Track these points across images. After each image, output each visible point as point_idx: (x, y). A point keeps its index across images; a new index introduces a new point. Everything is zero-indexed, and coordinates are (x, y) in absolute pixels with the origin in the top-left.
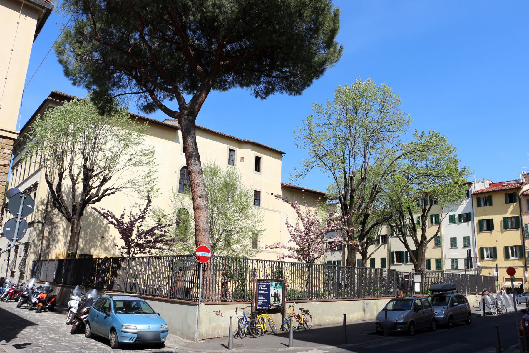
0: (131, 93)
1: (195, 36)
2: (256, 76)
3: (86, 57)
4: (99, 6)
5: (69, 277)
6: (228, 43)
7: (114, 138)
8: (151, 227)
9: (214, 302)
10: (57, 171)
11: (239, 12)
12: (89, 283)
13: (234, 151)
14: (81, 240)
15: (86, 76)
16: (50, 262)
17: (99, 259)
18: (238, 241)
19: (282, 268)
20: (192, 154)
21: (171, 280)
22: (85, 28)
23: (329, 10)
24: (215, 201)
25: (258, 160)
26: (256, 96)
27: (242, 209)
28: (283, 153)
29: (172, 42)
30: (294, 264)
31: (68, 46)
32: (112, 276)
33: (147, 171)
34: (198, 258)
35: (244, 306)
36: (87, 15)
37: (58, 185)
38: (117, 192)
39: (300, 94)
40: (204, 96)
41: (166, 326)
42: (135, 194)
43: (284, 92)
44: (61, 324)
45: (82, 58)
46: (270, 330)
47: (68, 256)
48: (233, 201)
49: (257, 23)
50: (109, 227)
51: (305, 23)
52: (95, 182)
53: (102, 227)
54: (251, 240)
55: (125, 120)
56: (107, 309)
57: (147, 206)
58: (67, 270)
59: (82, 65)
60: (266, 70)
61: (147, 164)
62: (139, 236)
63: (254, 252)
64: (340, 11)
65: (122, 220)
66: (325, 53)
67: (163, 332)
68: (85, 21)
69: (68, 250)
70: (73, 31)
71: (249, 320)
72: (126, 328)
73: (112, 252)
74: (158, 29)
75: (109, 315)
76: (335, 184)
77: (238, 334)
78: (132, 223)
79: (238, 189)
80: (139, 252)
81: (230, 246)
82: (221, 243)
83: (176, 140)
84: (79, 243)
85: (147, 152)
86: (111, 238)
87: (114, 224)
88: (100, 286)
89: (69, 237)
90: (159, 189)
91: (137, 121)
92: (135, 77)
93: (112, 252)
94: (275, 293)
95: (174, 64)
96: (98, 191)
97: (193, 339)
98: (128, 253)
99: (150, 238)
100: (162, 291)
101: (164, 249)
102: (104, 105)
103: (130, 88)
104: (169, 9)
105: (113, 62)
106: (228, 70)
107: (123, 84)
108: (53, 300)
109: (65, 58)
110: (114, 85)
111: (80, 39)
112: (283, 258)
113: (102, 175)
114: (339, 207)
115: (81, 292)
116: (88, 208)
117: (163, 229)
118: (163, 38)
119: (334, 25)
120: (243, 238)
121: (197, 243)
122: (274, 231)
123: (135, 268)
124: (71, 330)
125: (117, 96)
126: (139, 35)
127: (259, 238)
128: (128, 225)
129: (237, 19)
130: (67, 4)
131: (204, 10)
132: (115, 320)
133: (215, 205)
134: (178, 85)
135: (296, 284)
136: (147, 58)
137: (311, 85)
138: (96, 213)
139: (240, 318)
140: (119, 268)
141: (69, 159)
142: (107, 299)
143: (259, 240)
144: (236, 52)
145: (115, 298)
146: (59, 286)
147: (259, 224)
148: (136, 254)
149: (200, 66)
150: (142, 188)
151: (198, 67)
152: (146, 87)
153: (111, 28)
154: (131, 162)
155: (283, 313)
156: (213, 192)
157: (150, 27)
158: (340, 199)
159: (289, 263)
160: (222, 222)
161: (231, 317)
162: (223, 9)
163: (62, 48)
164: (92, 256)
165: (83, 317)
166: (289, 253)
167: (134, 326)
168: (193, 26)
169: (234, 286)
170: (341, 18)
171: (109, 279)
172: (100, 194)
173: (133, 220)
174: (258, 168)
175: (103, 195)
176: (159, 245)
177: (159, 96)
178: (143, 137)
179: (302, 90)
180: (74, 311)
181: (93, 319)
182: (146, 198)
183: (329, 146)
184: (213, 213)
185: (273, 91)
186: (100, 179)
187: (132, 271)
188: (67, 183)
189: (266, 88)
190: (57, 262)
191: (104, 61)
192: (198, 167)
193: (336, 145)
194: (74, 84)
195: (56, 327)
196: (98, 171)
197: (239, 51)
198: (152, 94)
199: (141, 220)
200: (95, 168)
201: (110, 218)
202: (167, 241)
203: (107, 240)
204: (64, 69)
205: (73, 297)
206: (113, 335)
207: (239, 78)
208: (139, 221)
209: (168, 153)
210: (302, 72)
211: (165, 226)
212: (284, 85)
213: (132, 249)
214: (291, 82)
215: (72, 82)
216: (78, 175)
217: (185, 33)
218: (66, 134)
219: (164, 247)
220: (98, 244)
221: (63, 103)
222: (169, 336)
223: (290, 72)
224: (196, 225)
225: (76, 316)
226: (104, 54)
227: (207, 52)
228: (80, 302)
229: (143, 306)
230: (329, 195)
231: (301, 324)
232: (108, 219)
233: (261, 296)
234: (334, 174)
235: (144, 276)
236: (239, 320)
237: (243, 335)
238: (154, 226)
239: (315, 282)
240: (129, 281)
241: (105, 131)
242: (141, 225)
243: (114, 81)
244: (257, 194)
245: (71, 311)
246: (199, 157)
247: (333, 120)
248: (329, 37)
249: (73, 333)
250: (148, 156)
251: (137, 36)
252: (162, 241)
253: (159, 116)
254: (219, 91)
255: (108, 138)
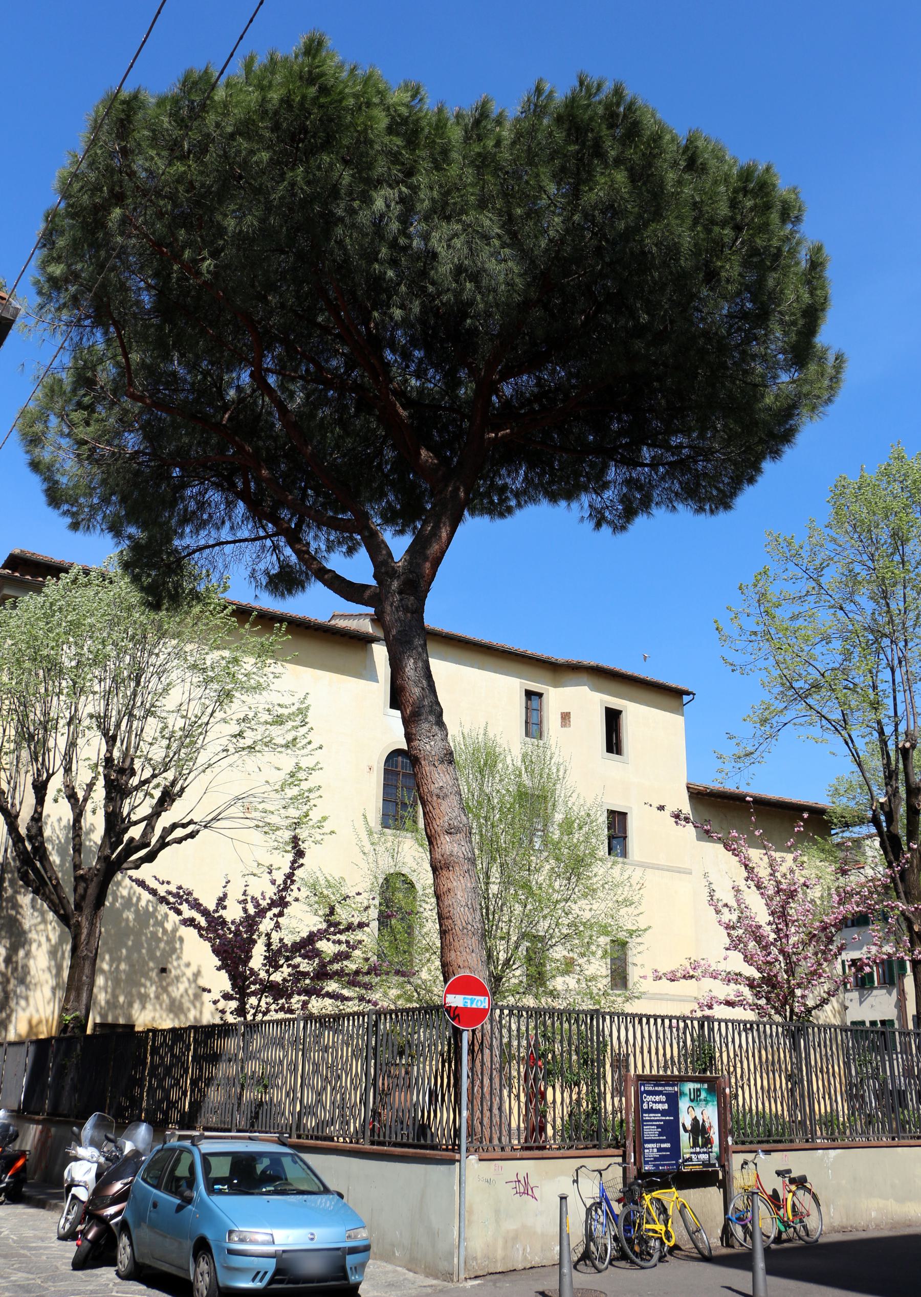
0: (234, 542)
1: (407, 366)
2: (592, 465)
3: (105, 449)
4: (138, 303)
5: (66, 1094)
6: (504, 377)
7: (188, 674)
8: (305, 934)
9: (508, 1153)
10: (30, 780)
11: (528, 285)
12: (126, 1109)
13: (540, 695)
14: (100, 981)
15: (105, 500)
16: (11, 1050)
17: (155, 1031)
18: (568, 967)
19: (711, 1038)
20: (415, 705)
21: (375, 1085)
22: (100, 368)
23: (793, 252)
24: (492, 849)
25: (613, 718)
26: (598, 525)
27: (576, 867)
28: (688, 693)
29: (342, 389)
30: (748, 1027)
31: (54, 421)
32: (194, 1083)
33: (289, 766)
34: (455, 1013)
35: (602, 1163)
36: (106, 333)
37: (33, 819)
38: (204, 833)
39: (727, 507)
40: (444, 535)
41: (363, 1234)
42: (256, 836)
43: (680, 507)
44: (42, 1239)
45: (93, 450)
46: (688, 1246)
47: (63, 1027)
48: (545, 843)
49: (583, 312)
50: (181, 940)
51: (724, 298)
52: (139, 806)
53: (160, 940)
54: (609, 961)
55: (218, 622)
56: (183, 1183)
57: (293, 868)
58: (61, 1072)
59: (95, 470)
60: (621, 446)
61: (287, 746)
62: (272, 961)
63: (620, 1000)
64: (826, 251)
65: (222, 912)
66: (794, 382)
67: (353, 1251)
68: (101, 347)
69: (64, 1010)
70: (67, 378)
71: (617, 1208)
72: (242, 1241)
73: (192, 1014)
74: (303, 354)
75: (189, 1201)
76: (857, 778)
77: (586, 1256)
78: (251, 923)
79: (560, 807)
80: (273, 1007)
81: (543, 984)
82: (516, 976)
83: (367, 672)
84: (95, 990)
85: (286, 712)
86: (189, 972)
87: (198, 927)
88: (160, 1116)
89: (66, 974)
90: (324, 819)
91: (254, 625)
92: (244, 495)
93: (192, 1014)
94: (695, 1120)
95: (354, 449)
96: (150, 827)
97: (448, 1276)
98: (241, 1011)
99: (305, 966)
100: (348, 1123)
101: (348, 999)
102: (161, 579)
103: (232, 528)
104: (332, 294)
105: (181, 457)
106: (509, 455)
107: (210, 516)
108: (20, 1163)
109: (46, 455)
110: (185, 520)
111: (86, 400)
112: (710, 1007)
113: (158, 786)
114: (873, 848)
115: (102, 1134)
116: (124, 885)
117: (343, 938)
118: (319, 377)
119: (812, 294)
120: (583, 955)
121: (446, 969)
122: (677, 927)
123: (264, 1055)
124: (72, 1255)
125: (194, 552)
126: (251, 375)
127: (630, 953)
128: (237, 930)
129: (526, 305)
130: (52, 306)
131: (431, 289)
132: (208, 1214)
133: (493, 859)
134: (368, 508)
135: (755, 1094)
136: (276, 439)
137: (759, 479)
138: (146, 896)
139: (589, 1202)
140: (215, 1058)
141: (62, 742)
142: (183, 1150)
143: (630, 959)
144: (529, 402)
145: (207, 1147)
146: (37, 1122)
147: (630, 910)
148: (265, 1014)
149: (428, 449)
150: (274, 819)
151: (424, 453)
152: (276, 521)
153: (172, 361)
154: (242, 743)
155: (724, 1185)
156: (486, 819)
157: (278, 350)
158: (875, 821)
159: (733, 1022)
160: (518, 909)
161: (563, 1198)
162: (485, 282)
163: (38, 427)
164: (133, 1026)
165: (112, 1210)
166: (729, 991)
167: (267, 1233)
168: (401, 337)
169: (567, 1100)
170: (830, 272)
171: (185, 1093)
172: (154, 841)
173: (252, 910)
174: (614, 744)
175: (163, 844)
176: (332, 986)
177: (313, 546)
178: (272, 669)
179: (733, 495)
180: (83, 1194)
181: (140, 1218)
182: (289, 848)
183: (828, 658)
184: (487, 884)
185: (646, 504)
186: (152, 796)
187: (253, 1067)
188: (58, 813)
189: (625, 500)
190: (32, 1049)
191: (154, 455)
192: (440, 744)
193: (847, 655)
194: (75, 526)
195: (30, 1249)
196: (147, 774)
197: (537, 398)
198: (294, 539)
199: (276, 910)
200: (137, 765)
201: (184, 907)
202: (357, 972)
203: (177, 978)
204: (45, 486)
205: (81, 1151)
206: (203, 1266)
207: (541, 475)
208: (269, 914)
209: (346, 716)
210: (728, 442)
211: (349, 928)
212: (677, 487)
213: (253, 1001)
214: (697, 476)
215: (68, 520)
216: (90, 786)
217: (381, 358)
218: (54, 669)
219: (346, 992)
220: (152, 991)
221: (43, 585)
222: (373, 1267)
223: (689, 447)
224: (441, 917)
225: (90, 1212)
226: (152, 434)
227: (445, 409)
228: (100, 1166)
229: (292, 1171)
230: (839, 810)
231: (787, 1225)
232: (179, 912)
233: (650, 1132)
234: (849, 742)
235: (290, 1080)
236: (589, 1211)
237: (602, 1260)
238: (315, 929)
239: (817, 1084)
240: (247, 1095)
241: (162, 657)
242: (277, 926)
243: (186, 510)
244: (617, 821)
245: (74, 1197)
246: (440, 714)
247: (831, 577)
248: (799, 333)
249: (81, 1263)
250: (290, 724)
251: (245, 378)
252: (339, 974)
253: (316, 603)
254: (486, 518)
255: (174, 676)
